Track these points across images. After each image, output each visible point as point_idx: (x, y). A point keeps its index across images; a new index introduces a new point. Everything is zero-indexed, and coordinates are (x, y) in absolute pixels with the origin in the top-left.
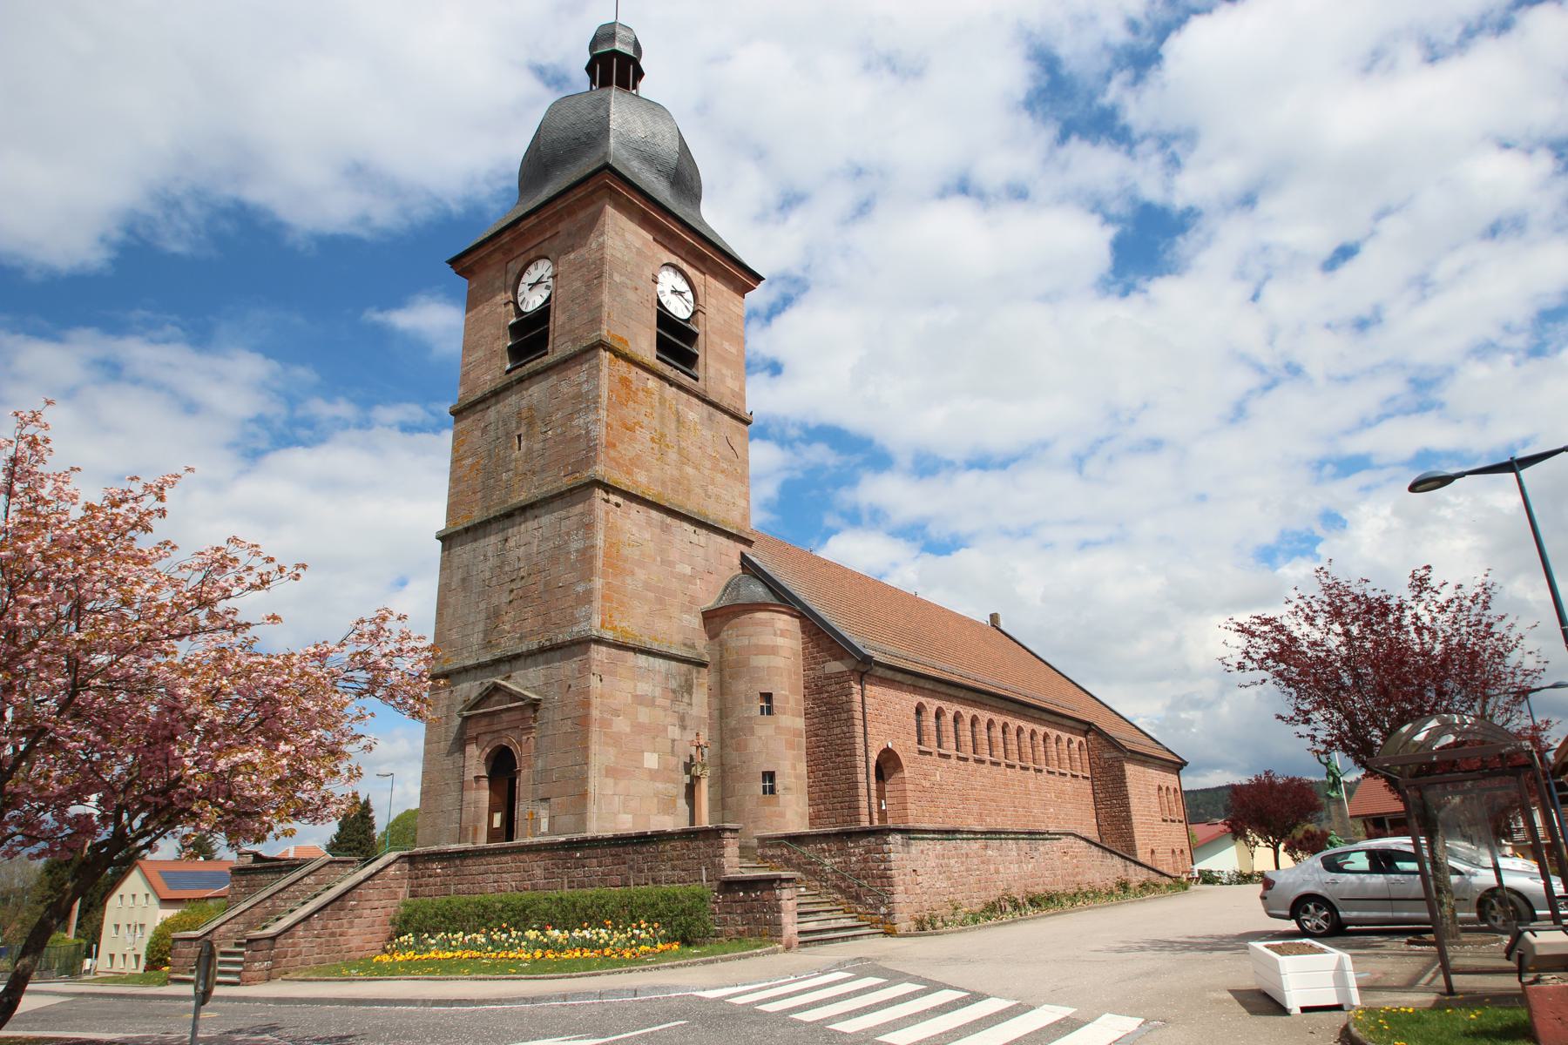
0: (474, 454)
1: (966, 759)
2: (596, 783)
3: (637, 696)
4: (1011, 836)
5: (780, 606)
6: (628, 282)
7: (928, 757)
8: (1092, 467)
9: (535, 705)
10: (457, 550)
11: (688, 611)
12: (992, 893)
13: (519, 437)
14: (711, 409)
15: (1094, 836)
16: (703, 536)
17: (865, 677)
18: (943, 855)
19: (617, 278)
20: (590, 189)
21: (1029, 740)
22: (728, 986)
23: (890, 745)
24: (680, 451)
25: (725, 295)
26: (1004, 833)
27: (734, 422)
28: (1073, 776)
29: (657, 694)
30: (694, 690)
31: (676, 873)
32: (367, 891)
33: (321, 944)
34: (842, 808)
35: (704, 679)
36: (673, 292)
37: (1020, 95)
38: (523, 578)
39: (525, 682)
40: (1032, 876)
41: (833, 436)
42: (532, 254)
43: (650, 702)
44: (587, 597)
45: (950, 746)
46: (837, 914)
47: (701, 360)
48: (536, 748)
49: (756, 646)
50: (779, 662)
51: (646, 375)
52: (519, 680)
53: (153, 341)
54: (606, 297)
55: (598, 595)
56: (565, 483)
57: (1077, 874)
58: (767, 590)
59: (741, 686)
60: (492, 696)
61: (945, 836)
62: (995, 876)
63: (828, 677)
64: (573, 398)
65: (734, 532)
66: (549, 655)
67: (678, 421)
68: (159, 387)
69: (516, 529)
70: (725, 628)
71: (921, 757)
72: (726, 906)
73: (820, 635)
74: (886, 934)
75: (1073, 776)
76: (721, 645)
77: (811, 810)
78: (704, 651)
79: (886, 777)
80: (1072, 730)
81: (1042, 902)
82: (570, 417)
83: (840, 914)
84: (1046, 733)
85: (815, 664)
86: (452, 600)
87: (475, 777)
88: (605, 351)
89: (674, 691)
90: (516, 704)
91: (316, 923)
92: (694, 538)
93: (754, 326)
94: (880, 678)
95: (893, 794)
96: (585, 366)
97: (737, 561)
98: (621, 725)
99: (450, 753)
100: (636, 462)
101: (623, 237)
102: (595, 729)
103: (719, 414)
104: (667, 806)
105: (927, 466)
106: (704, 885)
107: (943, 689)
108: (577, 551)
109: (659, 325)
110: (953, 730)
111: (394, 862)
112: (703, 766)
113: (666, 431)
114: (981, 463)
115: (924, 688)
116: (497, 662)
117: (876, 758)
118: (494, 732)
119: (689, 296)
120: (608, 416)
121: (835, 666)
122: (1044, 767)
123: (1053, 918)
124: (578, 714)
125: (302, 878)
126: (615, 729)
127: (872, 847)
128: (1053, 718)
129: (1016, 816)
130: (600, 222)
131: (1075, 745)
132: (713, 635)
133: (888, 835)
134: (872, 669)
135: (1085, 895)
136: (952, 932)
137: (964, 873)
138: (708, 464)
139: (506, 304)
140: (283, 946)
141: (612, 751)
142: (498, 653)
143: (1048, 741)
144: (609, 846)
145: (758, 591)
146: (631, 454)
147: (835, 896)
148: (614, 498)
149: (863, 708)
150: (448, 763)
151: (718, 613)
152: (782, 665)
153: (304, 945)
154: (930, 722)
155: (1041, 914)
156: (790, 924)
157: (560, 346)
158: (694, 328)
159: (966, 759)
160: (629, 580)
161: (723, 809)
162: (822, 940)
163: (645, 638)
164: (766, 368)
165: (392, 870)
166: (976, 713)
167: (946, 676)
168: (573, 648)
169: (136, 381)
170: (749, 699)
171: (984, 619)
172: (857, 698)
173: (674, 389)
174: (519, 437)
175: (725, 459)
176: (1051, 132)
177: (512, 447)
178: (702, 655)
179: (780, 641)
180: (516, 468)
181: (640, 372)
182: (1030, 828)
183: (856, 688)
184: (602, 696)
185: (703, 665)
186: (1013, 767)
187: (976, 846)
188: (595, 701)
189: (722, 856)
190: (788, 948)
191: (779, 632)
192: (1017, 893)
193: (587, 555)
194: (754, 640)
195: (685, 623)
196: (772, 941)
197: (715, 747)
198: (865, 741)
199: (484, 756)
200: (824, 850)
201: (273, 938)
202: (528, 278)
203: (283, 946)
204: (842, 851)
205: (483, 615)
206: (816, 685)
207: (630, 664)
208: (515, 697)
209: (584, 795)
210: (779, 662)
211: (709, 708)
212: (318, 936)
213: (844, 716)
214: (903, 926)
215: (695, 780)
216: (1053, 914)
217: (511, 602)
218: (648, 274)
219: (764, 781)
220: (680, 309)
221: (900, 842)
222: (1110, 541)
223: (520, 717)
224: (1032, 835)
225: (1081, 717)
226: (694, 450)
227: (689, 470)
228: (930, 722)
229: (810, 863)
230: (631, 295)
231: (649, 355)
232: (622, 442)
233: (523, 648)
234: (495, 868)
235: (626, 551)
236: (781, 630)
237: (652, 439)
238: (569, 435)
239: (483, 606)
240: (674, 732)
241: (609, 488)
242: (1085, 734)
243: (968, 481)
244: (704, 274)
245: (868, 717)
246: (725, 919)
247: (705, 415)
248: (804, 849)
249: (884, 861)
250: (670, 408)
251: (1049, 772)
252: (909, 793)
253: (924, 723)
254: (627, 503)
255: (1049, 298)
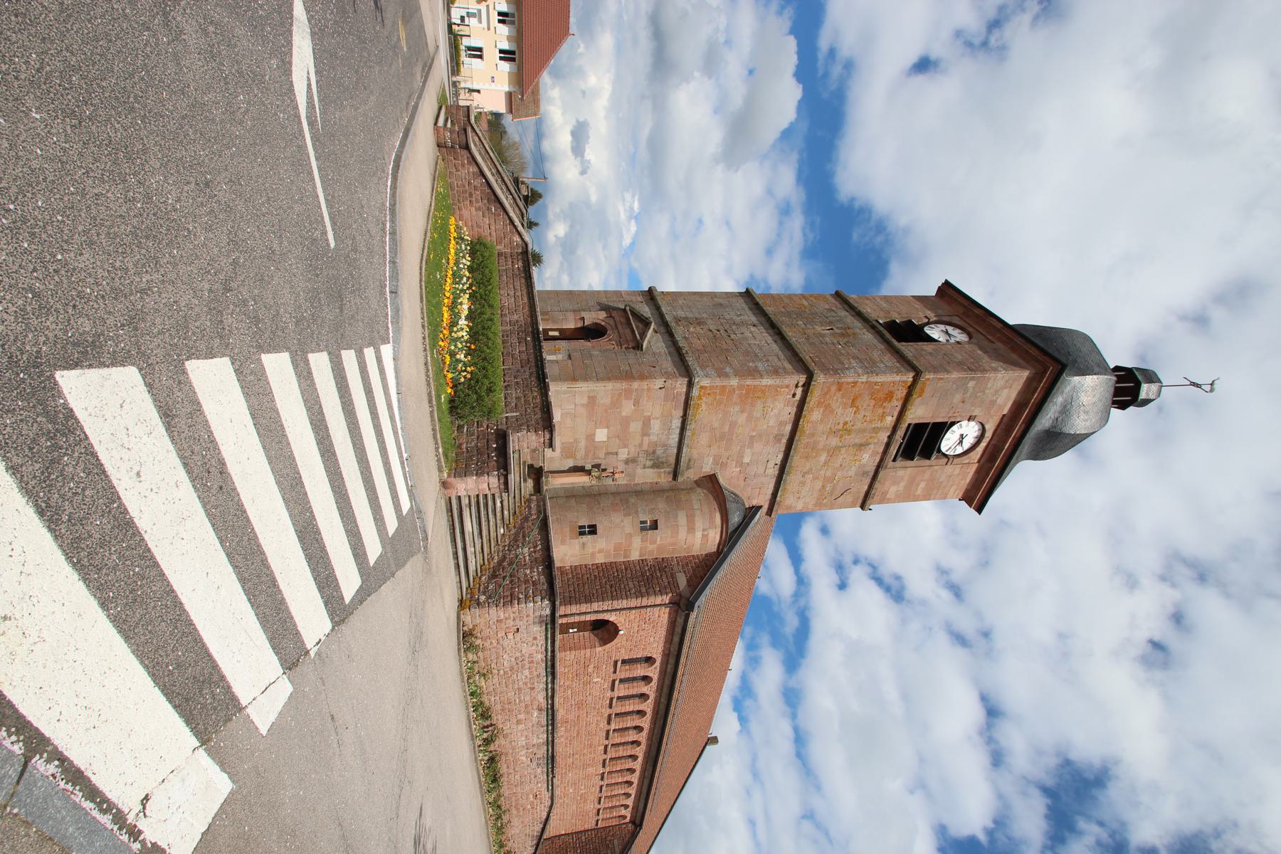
0: (811, 306)
1: (610, 706)
2: (584, 387)
3: (649, 420)
4: (550, 736)
5: (727, 532)
6: (968, 394)
7: (612, 670)
8: (807, 826)
9: (638, 347)
10: (741, 300)
11: (716, 462)
12: (500, 717)
13: (832, 329)
14: (871, 474)
15: (551, 831)
16: (773, 471)
17: (676, 607)
18: (532, 662)
19: (971, 384)
20: (1039, 357)
21: (627, 767)
22: (398, 384)
23: (621, 632)
24: (838, 448)
25: (963, 482)
26: (553, 729)
27: (862, 495)
28: (599, 810)
29: (651, 437)
30: (655, 470)
31: (514, 400)
32: (502, 221)
33: (464, 186)
34: (570, 591)
35: (664, 478)
36: (962, 435)
37: (1073, 756)
38: (729, 336)
39: (653, 340)
40: (516, 761)
41: (804, 631)
42: (970, 329)
43: (645, 432)
44: (721, 374)
45: (621, 690)
46: (479, 556)
47: (909, 463)
48: (607, 350)
49: (693, 516)
50: (683, 534)
51: (896, 414)
52: (655, 338)
53: (804, 229)
54: (955, 375)
55: (725, 382)
56: (807, 358)
57: (518, 809)
58: (736, 526)
59: (661, 505)
60: (642, 323)
61: (549, 663)
62: (515, 721)
63: (673, 576)
64: (870, 359)
65: (778, 499)
66: (676, 354)
67: (861, 445)
68: (779, 235)
69: (764, 330)
70: (705, 491)
71: (612, 663)
72: (484, 435)
73: (705, 568)
74: (461, 601)
75: (599, 810)
76: (691, 488)
77: (567, 568)
78: (685, 477)
79: (595, 632)
80: (635, 808)
81: (492, 772)
82: (855, 358)
83: (480, 561)
84: (633, 783)
85: (683, 566)
86: (705, 299)
87: (583, 317)
88: (913, 377)
89: (654, 452)
90: (638, 335)
91: (479, 181)
92: (771, 464)
93: (869, 569)
94: (675, 621)
95: (581, 638)
96: (898, 365)
97: (755, 502)
98: (627, 408)
99: (599, 304)
100: (828, 410)
101: (1004, 387)
102: (623, 385)
103: (867, 481)
104: (568, 452)
105: (792, 698)
106: (505, 415)
107: (667, 682)
108: (756, 367)
109: (935, 424)
110: (634, 693)
111: (522, 239)
112: (599, 478)
113: (853, 435)
114: (800, 739)
115: (667, 663)
116: (665, 324)
117: (611, 619)
118: (616, 325)
119: (959, 450)
120: (863, 383)
121: (682, 581)
122: (606, 782)
123: (477, 781)
124: (634, 373)
125: (511, 194)
126: (624, 402)
127: (538, 586)
128: (645, 791)
129: (566, 756)
130: (1014, 368)
131: (623, 812)
132: (698, 483)
133: (550, 600)
134: (683, 611)
135: (499, 817)
136: (461, 665)
137: (516, 686)
138: (829, 473)
139: (926, 317)
140: (462, 157)
141: (607, 401)
142: (673, 324)
143: (626, 785)
144: (536, 357)
145: (735, 519)
146: (834, 406)
147: (496, 557)
148: (799, 391)
149: (651, 606)
150: (592, 303)
151: (716, 485)
152: (680, 537)
153: (463, 172)
154: (640, 671)
155: (481, 768)
156: (468, 487)
157: (908, 349)
158: (933, 457)
159: (610, 706)
160: (737, 408)
161: (566, 497)
162: (454, 529)
163: (693, 426)
164: (841, 580)
165: (517, 238)
166: (648, 715)
167: (677, 685)
168: (683, 368)
169: (781, 223)
170: (652, 511)
171: (714, 732)
172: (659, 600)
173: (886, 440)
174: (832, 329)
175: (834, 488)
176: (1050, 782)
177: (822, 325)
178: (683, 475)
179: (699, 534)
180: (809, 329)
181: (898, 409)
182: (558, 759)
183: (666, 599)
184: (649, 389)
185: (675, 477)
186: (605, 752)
187: (541, 698)
188: (645, 384)
189: (529, 431)
190: (445, 485)
191: (706, 533)
192: (498, 745)
193: (754, 373)
194: (698, 513)
195: (706, 459)
196: (450, 470)
197: (613, 489)
198: (624, 609)
199: (598, 321)
200: (535, 547)
201: (467, 148)
202: (950, 329)
203: (462, 157)
204: (534, 561)
205: (698, 316)
206: (666, 567)
207: (674, 412)
208: (643, 335)
209: (574, 379)
210: (683, 534)
211: (642, 483)
212: (469, 183)
213: (643, 590)
214: (467, 618)
215: (589, 473)
216: (478, 773)
217: (711, 331)
218: (976, 412)
219: (590, 526)
220: (949, 443)
221: (543, 613)
222: (757, 844)
223: (629, 339)
224: (551, 760)
225: (646, 817)
226: (839, 461)
227: (823, 457)
228: (640, 671)
229: (524, 537)
230: (958, 398)
231: (911, 417)
232: (843, 397)
233: (678, 338)
234: (519, 293)
235: (759, 405)
236: (707, 535)
237: (846, 423)
238: (842, 358)
239: (705, 315)
240: (623, 454)
241: (807, 386)
242: (632, 822)
243: (786, 728)
244: (979, 462)
245: (643, 611)
246: (473, 435)
247: (867, 469)
248: (536, 531)
249: (526, 597)
250: (871, 437)
251: (601, 787)
252: (583, 652)
253: (639, 666)
254: (796, 404)
255: (920, 785)
